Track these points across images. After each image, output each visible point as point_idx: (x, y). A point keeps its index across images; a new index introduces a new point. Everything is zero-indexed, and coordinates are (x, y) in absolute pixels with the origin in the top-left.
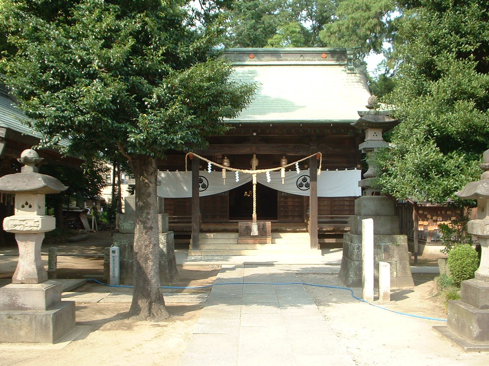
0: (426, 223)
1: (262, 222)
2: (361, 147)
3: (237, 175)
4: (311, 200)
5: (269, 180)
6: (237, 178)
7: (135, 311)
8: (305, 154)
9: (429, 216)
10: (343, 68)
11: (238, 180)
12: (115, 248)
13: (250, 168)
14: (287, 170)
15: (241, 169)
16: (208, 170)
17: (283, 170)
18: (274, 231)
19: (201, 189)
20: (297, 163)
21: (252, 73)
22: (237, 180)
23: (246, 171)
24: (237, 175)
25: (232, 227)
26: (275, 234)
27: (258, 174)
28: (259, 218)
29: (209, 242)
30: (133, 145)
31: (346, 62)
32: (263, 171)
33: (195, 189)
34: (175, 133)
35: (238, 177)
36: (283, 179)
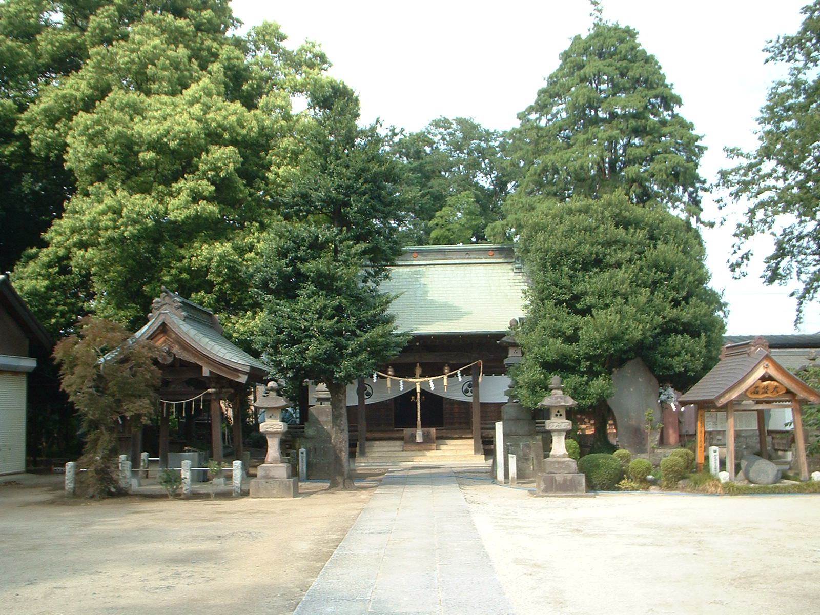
0: (583, 427)
2: (506, 361)
3: (401, 383)
4: (778, 352)
5: (433, 388)
6: (402, 386)
7: (330, 488)
8: (467, 361)
9: (586, 420)
10: (510, 267)
12: (303, 450)
13: (413, 376)
14: (449, 377)
15: (405, 377)
17: (445, 378)
18: (438, 438)
19: (366, 397)
20: (459, 371)
21: (416, 273)
22: (402, 389)
23: (411, 380)
24: (401, 383)
25: (398, 435)
26: (440, 441)
27: (421, 382)
28: (423, 426)
29: (375, 449)
30: (337, 378)
31: (514, 260)
32: (426, 379)
33: (361, 400)
34: (362, 370)
35: (402, 384)
36: (447, 385)
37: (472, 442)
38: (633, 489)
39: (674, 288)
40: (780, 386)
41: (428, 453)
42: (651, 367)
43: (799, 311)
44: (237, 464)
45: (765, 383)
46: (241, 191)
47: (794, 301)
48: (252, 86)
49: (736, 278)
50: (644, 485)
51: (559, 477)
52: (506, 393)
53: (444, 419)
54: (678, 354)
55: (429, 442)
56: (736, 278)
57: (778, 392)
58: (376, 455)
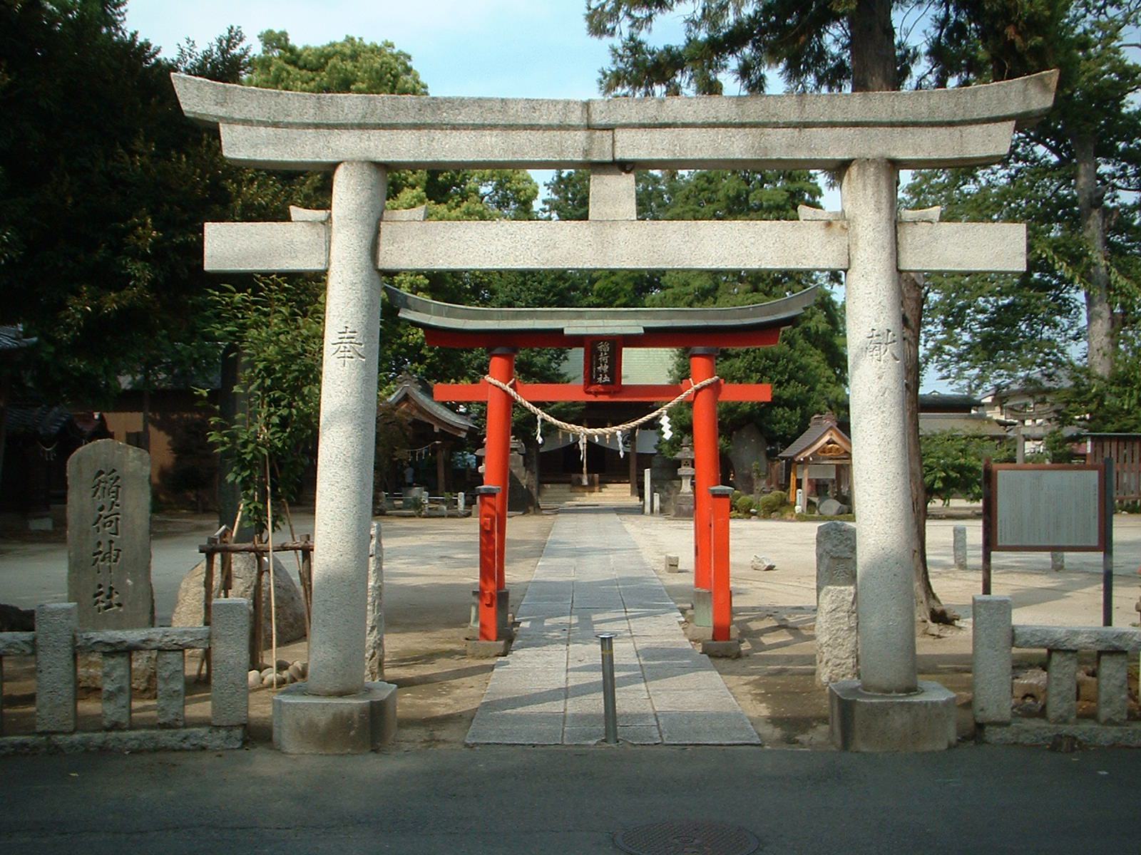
1: (590, 475)
11: (671, 433)
16: (663, 433)
28: (588, 472)
37: (629, 486)
38: (739, 518)
39: (779, 373)
41: (594, 495)
42: (761, 429)
44: (461, 494)
46: (448, 282)
48: (446, 178)
50: (747, 515)
51: (684, 507)
52: (656, 447)
53: (606, 466)
54: (779, 423)
55: (591, 487)
58: (549, 495)
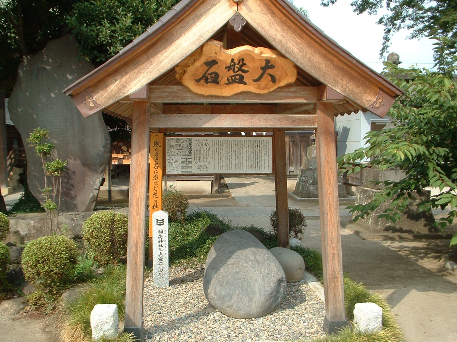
40: (280, 61)
43: (387, 39)
45: (236, 51)
47: (382, 27)
49: (325, 5)
56: (325, 5)
57: (274, 79)
